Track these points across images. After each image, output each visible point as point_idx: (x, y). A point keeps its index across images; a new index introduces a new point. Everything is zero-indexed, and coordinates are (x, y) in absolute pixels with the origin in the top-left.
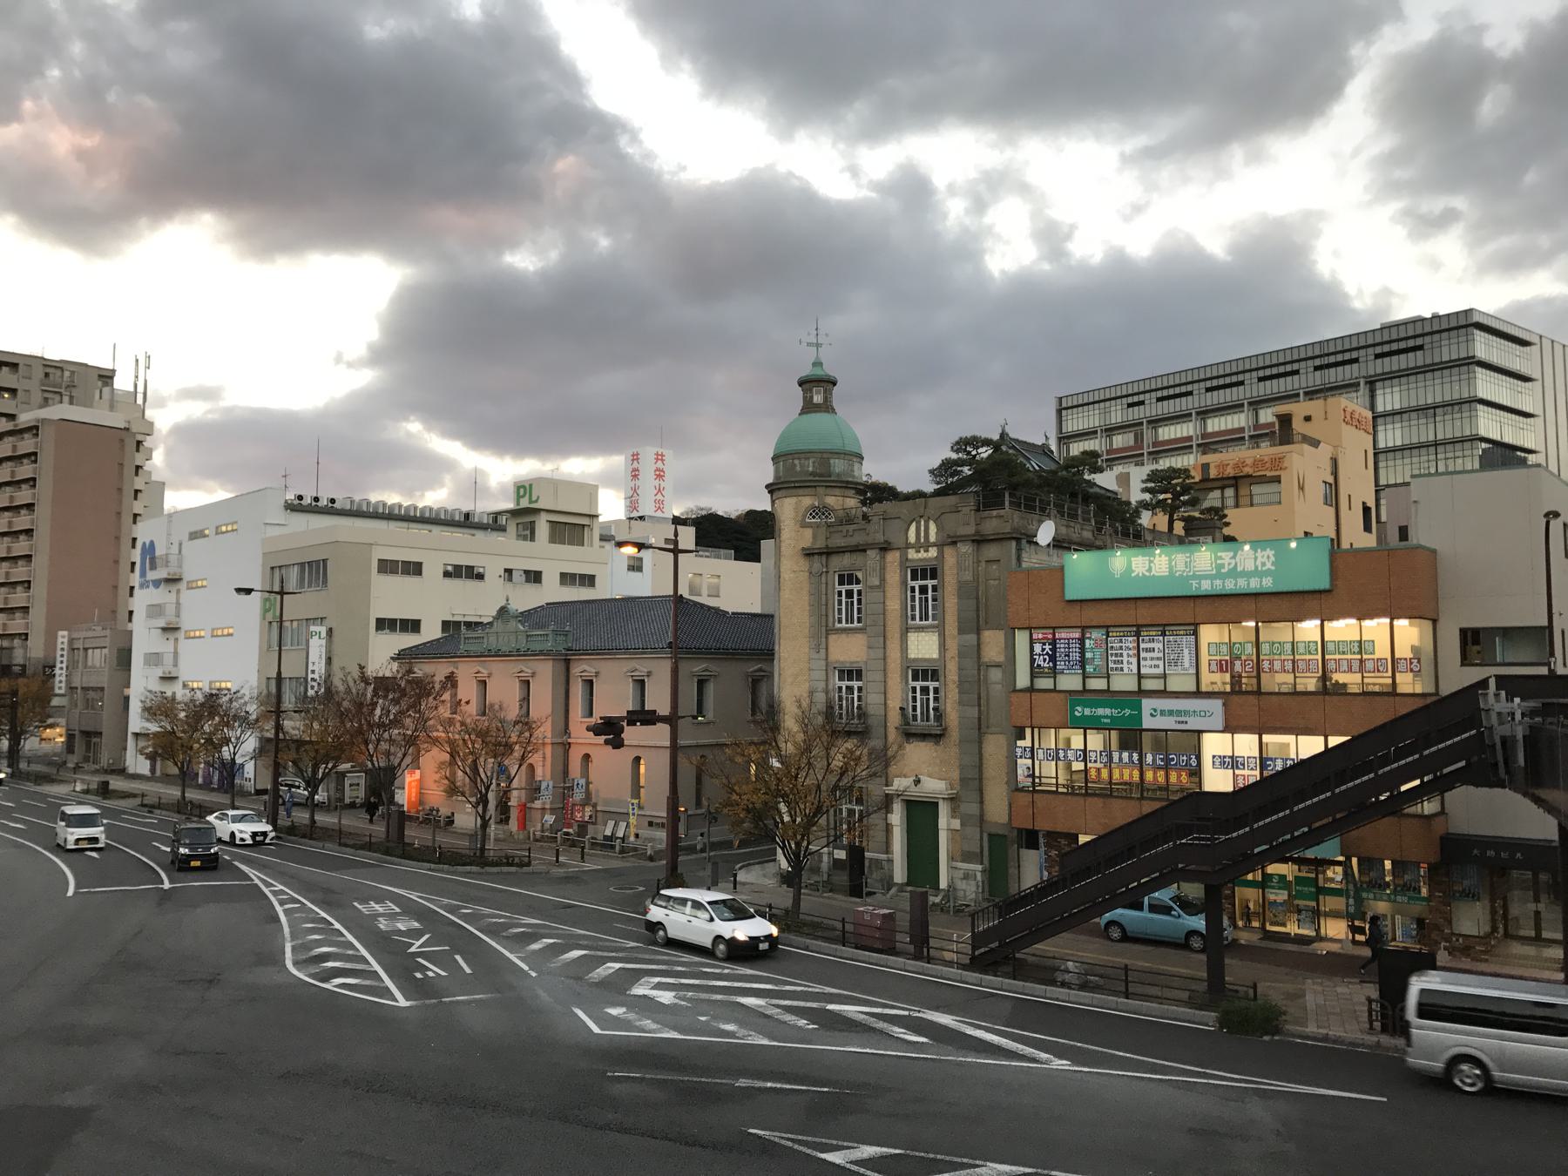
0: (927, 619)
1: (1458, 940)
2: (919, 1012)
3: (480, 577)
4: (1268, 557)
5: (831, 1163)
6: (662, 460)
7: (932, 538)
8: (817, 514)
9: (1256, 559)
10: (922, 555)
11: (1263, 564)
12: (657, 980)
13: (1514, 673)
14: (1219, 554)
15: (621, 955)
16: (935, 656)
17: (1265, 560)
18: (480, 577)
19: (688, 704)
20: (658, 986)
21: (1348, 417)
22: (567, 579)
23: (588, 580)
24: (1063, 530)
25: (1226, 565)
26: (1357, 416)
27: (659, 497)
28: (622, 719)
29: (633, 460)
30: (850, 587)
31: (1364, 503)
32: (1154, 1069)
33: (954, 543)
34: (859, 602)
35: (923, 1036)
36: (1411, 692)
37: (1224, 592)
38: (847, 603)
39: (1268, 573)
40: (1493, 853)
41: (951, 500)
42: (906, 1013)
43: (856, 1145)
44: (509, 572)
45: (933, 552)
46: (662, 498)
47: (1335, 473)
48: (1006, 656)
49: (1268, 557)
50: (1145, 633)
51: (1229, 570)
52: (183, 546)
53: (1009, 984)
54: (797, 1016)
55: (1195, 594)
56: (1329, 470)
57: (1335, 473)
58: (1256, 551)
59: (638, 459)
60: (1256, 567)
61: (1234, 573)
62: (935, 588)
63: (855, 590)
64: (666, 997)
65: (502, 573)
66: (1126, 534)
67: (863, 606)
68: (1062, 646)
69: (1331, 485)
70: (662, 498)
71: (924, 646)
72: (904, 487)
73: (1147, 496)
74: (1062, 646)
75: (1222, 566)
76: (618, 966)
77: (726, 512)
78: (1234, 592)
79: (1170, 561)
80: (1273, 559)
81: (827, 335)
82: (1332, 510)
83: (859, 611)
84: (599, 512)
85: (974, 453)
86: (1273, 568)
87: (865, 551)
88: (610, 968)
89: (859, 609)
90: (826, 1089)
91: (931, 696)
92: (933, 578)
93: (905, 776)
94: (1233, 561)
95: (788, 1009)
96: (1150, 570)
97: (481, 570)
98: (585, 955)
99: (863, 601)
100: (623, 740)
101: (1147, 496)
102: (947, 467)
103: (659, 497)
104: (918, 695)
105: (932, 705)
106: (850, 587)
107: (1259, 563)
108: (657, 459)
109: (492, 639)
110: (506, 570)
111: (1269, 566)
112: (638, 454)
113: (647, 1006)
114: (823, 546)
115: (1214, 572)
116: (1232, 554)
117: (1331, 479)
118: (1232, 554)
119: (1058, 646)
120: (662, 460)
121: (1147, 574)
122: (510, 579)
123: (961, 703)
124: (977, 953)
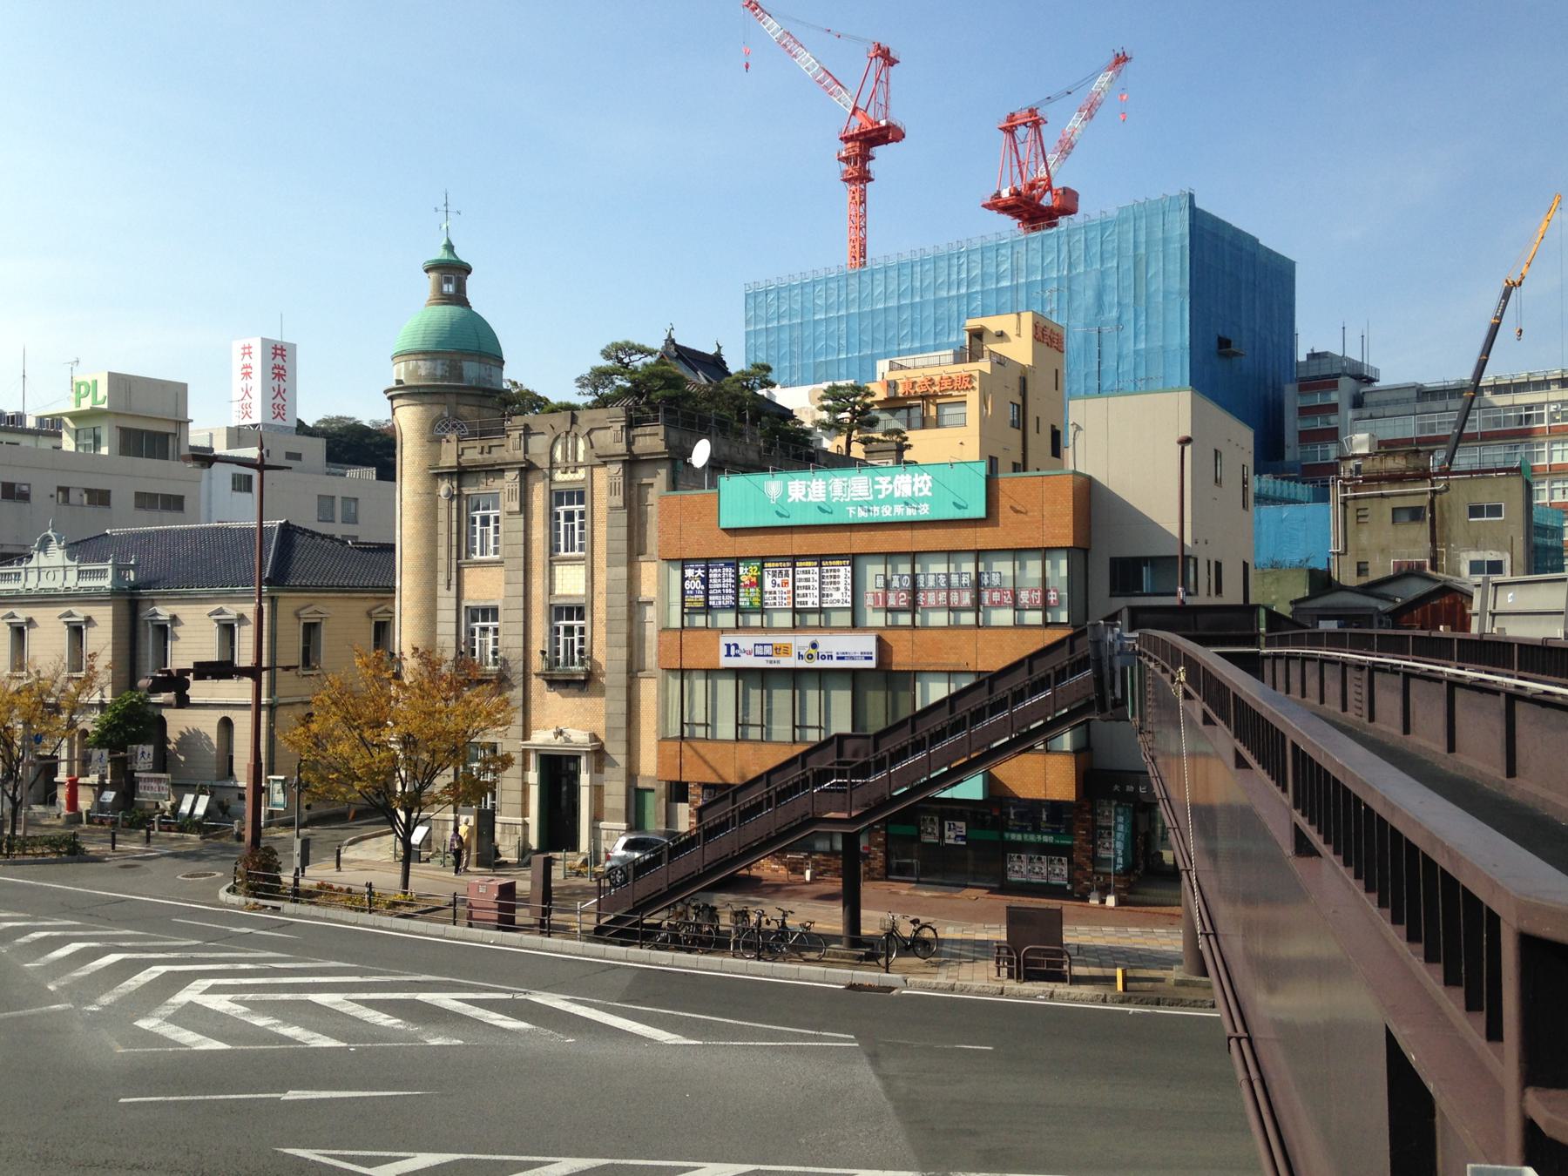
0: (573, 550)
1: (1098, 879)
2: (525, 993)
3: (25, 497)
4: (925, 483)
5: (745, 1163)
6: (283, 356)
7: (581, 458)
8: (447, 426)
9: (913, 484)
10: (569, 476)
11: (920, 490)
12: (211, 982)
13: (1161, 604)
14: (877, 479)
15: (172, 955)
16: (582, 591)
17: (922, 485)
18: (25, 497)
19: (291, 651)
20: (214, 990)
21: (1040, 334)
22: (145, 501)
23: (174, 503)
24: (725, 450)
25: (883, 491)
26: (1048, 333)
27: (279, 400)
28: (187, 672)
29: (244, 354)
30: (570, 507)
31: (1053, 426)
32: (771, 1036)
33: (605, 464)
34: (497, 529)
35: (522, 1020)
36: (522, 637)
37: (880, 520)
38: (566, 527)
39: (924, 499)
40: (1132, 788)
41: (601, 414)
42: (510, 996)
43: (412, 1154)
44: (65, 490)
45: (582, 474)
46: (282, 402)
47: (1024, 394)
48: (658, 592)
49: (925, 483)
50: (769, 565)
51: (887, 496)
52: (541, 436)
53: (635, 953)
54: (378, 1010)
55: (851, 522)
56: (1017, 390)
57: (1024, 394)
58: (913, 476)
59: (250, 353)
60: (913, 493)
61: (891, 500)
62: (582, 515)
63: (492, 516)
64: (219, 1003)
65: (54, 492)
66: (798, 457)
67: (501, 535)
68: (715, 576)
69: (1018, 406)
70: (282, 402)
71: (570, 582)
72: (555, 399)
73: (824, 416)
74: (715, 576)
75: (879, 491)
76: (163, 969)
77: (375, 423)
78: (890, 520)
79: (827, 485)
80: (930, 484)
81: (436, 210)
82: (1019, 433)
83: (496, 540)
84: (189, 417)
85: (626, 360)
86: (930, 494)
87: (503, 471)
88: (154, 972)
89: (581, 535)
90: (292, 1095)
91: (576, 637)
92: (581, 501)
93: (545, 728)
94: (890, 487)
95: (369, 1004)
96: (806, 496)
97: (25, 488)
98: (123, 960)
99: (501, 529)
100: (188, 697)
101: (824, 416)
102: (600, 377)
103: (279, 400)
104: (561, 636)
105: (576, 647)
106: (570, 507)
107: (916, 489)
108: (276, 354)
109: (33, 576)
110: (60, 489)
111: (926, 492)
112: (250, 347)
113: (192, 1016)
114: (455, 464)
115: (871, 498)
116: (889, 478)
117: (1019, 401)
118: (889, 478)
119: (710, 576)
120: (283, 356)
121: (804, 499)
122: (66, 501)
123: (608, 645)
124: (603, 921)
